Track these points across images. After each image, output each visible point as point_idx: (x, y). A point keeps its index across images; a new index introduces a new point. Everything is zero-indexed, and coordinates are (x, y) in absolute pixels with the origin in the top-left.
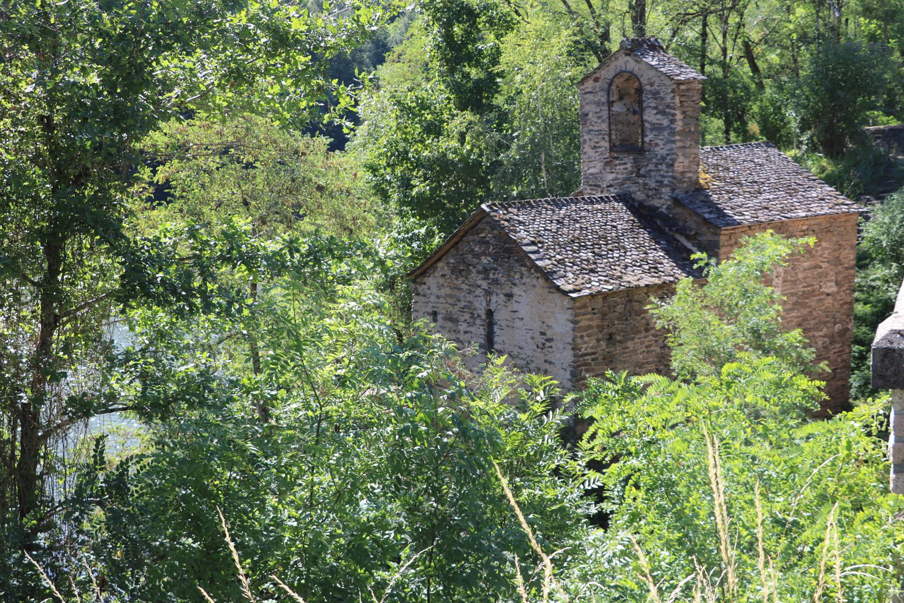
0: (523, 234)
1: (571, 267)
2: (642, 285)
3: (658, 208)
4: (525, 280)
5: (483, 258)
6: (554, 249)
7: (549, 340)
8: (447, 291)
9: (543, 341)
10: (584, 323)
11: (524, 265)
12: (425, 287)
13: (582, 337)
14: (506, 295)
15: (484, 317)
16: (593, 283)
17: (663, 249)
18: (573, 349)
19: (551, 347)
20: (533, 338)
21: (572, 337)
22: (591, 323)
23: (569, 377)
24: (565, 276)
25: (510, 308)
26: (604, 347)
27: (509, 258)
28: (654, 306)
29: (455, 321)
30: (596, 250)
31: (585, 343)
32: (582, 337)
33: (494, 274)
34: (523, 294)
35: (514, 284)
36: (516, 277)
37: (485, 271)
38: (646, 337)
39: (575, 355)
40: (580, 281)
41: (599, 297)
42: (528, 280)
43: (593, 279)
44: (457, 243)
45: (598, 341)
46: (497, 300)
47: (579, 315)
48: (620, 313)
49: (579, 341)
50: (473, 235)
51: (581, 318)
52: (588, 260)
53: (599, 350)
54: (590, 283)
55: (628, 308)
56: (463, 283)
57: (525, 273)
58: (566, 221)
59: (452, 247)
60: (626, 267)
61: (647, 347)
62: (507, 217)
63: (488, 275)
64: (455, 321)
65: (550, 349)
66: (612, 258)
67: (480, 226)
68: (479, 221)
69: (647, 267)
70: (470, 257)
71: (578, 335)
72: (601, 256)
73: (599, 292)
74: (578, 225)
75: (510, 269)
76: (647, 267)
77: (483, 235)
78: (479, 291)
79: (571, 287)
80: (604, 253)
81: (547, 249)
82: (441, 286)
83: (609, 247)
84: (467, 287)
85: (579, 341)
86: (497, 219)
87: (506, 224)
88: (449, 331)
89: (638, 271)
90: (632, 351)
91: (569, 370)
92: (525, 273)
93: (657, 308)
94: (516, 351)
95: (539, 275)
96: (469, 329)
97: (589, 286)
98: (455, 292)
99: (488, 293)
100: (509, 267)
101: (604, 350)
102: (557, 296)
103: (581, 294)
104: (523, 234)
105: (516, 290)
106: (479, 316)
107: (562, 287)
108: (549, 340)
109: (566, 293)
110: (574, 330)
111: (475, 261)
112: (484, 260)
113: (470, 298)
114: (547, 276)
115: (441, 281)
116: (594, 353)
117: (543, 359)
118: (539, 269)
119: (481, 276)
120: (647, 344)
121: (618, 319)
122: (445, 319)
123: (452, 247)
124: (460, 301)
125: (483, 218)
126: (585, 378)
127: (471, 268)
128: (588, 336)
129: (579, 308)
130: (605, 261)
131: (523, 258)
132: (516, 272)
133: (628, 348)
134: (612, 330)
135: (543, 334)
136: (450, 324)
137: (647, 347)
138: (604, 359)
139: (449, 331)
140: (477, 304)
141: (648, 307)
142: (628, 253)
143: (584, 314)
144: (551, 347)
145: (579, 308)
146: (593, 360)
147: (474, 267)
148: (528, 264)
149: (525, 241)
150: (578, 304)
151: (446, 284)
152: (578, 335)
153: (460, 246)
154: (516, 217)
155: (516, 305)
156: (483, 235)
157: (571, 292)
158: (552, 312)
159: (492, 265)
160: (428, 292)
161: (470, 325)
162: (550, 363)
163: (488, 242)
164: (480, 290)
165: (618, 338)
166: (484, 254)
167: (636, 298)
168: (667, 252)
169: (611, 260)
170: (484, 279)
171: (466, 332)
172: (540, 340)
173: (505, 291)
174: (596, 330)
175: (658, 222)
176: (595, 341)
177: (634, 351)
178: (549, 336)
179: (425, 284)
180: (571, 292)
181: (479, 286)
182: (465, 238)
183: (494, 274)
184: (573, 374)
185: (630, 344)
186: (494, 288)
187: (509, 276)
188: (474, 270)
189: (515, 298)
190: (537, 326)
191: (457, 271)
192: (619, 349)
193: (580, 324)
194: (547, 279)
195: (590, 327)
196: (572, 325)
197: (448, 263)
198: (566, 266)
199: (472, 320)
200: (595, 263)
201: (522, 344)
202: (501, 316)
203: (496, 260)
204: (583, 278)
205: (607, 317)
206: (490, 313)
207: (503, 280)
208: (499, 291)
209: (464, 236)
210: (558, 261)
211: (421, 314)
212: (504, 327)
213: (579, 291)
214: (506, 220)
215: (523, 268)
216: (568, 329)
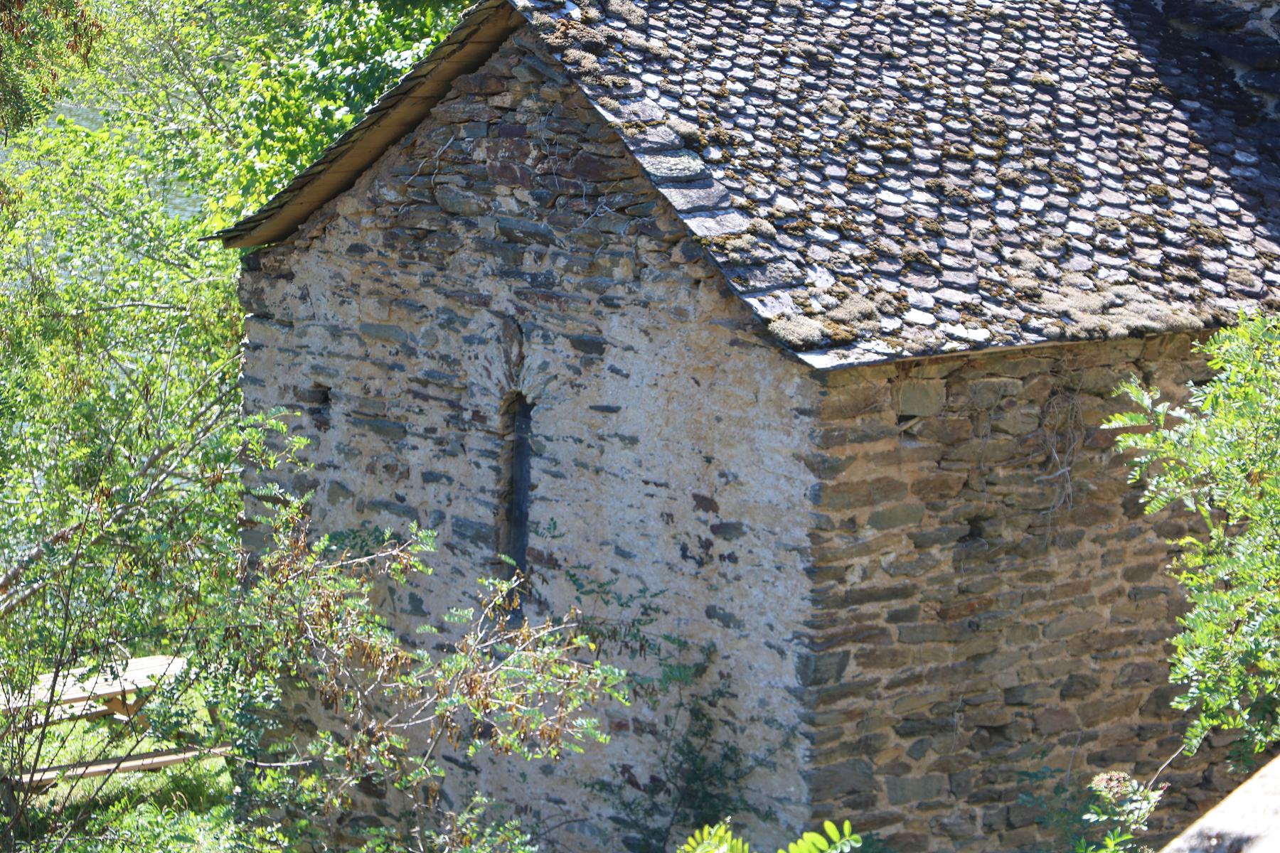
0: (652, 106)
1: (832, 246)
2: (1117, 329)
3: (1244, 16)
4: (648, 288)
5: (502, 189)
6: (772, 174)
7: (725, 530)
8: (364, 310)
9: (706, 534)
10: (858, 473)
11: (648, 230)
12: (291, 288)
13: (852, 525)
14: (579, 343)
15: (496, 422)
16: (913, 315)
17: (1237, 185)
18: (810, 572)
19: (732, 558)
20: (668, 518)
21: (811, 523)
22: (891, 472)
23: (794, 682)
24: (801, 283)
25: (590, 396)
26: (947, 568)
27: (593, 197)
28: (1141, 420)
29: (393, 430)
30: (951, 182)
31: (866, 549)
32: (852, 525)
33: (540, 257)
34: (640, 342)
35: (611, 303)
36: (618, 273)
37: (509, 243)
38: (1129, 536)
39: (818, 598)
40: (858, 303)
41: (932, 370)
42: (659, 290)
43: (913, 297)
44: (411, 126)
45: (920, 543)
46: (547, 357)
47: (842, 440)
48: (1022, 439)
49: (837, 541)
50: (469, 96)
51: (849, 450)
52: (906, 222)
53: (922, 579)
54: (898, 313)
55: (1056, 417)
56: (425, 284)
57: (651, 259)
58: (844, 63)
59: (395, 141)
60: (1067, 252)
61: (1130, 575)
62: (599, 34)
63: (519, 260)
64: (393, 430)
65: (727, 567)
66: (1015, 216)
67: (496, 64)
68: (495, 45)
69: (1154, 257)
70: (455, 182)
71: (836, 517)
72: (965, 205)
73: (930, 354)
74: (891, 78)
75: (599, 240)
76: (1154, 257)
77: (506, 100)
78: (481, 321)
79: (812, 328)
80: (981, 193)
81: (744, 172)
82: (345, 292)
83: (1009, 169)
84: (441, 302)
85: (837, 541)
86: (552, 39)
87: (589, 61)
88: (371, 469)
89: (1112, 271)
90: (1068, 589)
91: (794, 651)
92: (651, 259)
93: (1153, 428)
94: (603, 564)
95: (699, 273)
96: (439, 466)
97: (890, 324)
98: (399, 319)
99: (515, 330)
100: (593, 232)
101: (944, 580)
102: (760, 357)
103: (854, 356)
104: (652, 106)
105: (615, 328)
106: (478, 416)
107: (776, 326)
108: (725, 530)
109: (790, 350)
110: (817, 496)
111: (474, 201)
112: (508, 200)
113: (450, 344)
114: (727, 275)
115: (350, 270)
116: (903, 593)
117: (702, 602)
118: (697, 249)
119: (494, 262)
120: (1132, 562)
121: (1010, 460)
122: (358, 418)
123: (395, 141)
124: (411, 352)
125: (512, 30)
126: (237, 822)
127: (457, 226)
128: (877, 521)
129: (841, 412)
130: (983, 225)
131: (643, 205)
132: (616, 255)
133: (1049, 576)
134: (983, 503)
135: (705, 503)
136: (373, 442)
137: (1130, 575)
138: (942, 615)
139: (371, 469)
140: (472, 372)
141: (1118, 421)
142: (1087, 199)
143: (864, 438)
144: (732, 558)
145: (841, 412)
146: (894, 617)
147: (470, 225)
148: (662, 225)
149: (656, 136)
150: (837, 397)
151: (366, 285)
152: (836, 517)
153: (420, 136)
154: (635, 38)
155: (611, 382)
156: (506, 100)
157: (810, 346)
158: (742, 422)
159: (531, 223)
160: (302, 310)
161: (446, 449)
162: (728, 620)
163: (520, 131)
164: (485, 316)
165: (1008, 535)
166: (506, 174)
167: (1090, 378)
168: (1257, 199)
169: (1006, 224)
170: (503, 274)
171: (430, 477)
172: (694, 525)
173: (574, 328)
174: (912, 500)
175: (1239, 74)
176: (906, 545)
177: (1077, 589)
178: (726, 514)
179: (289, 276)
180: (810, 346)
181: (485, 302)
182: (438, 110)
183: (540, 257)
184: (807, 670)
185: (1057, 561)
186: (538, 312)
187: (592, 266)
188: (467, 237)
189: (612, 357)
190: (685, 471)
191: (406, 237)
192: (1008, 580)
193: (843, 476)
194: (727, 293)
195: (888, 488)
196: (812, 479)
197: (375, 203)
198: (809, 241)
199: (452, 433)
200: (935, 235)
201: (629, 538)
202: (555, 423)
203: (547, 203)
204: (870, 295)
205: (962, 450)
206: (519, 409)
207: (570, 283)
208: (553, 325)
209: (438, 97)
210: (780, 222)
211: (272, 391)
212: (567, 466)
213: (847, 344)
214: (592, 47)
215: (643, 241)
216: (797, 492)
